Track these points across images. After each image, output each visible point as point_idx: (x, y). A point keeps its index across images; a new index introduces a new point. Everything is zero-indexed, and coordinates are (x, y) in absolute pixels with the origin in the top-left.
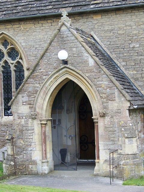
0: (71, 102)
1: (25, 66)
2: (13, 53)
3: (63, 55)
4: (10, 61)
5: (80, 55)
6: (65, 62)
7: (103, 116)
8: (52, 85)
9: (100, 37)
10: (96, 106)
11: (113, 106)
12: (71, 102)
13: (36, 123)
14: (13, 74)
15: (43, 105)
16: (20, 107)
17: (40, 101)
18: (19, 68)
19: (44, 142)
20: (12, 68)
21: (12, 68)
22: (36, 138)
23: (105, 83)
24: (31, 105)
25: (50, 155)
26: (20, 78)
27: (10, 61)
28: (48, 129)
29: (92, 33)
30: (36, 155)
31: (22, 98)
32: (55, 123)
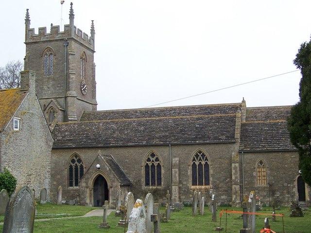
0: (100, 181)
1: (84, 166)
2: (79, 161)
3: (98, 166)
4: (78, 164)
5: (104, 166)
6: (99, 168)
7: (111, 187)
8: (94, 176)
9: (114, 157)
10: (109, 184)
11: (115, 184)
12: (100, 181)
13: (88, 189)
14: (74, 170)
15: (91, 183)
16: (83, 184)
17: (90, 181)
18: (82, 167)
19: (91, 196)
20: (74, 167)
21: (79, 167)
22: (88, 195)
23: (112, 176)
24: (87, 183)
25: (92, 201)
26: (82, 175)
27: (78, 164)
28: (92, 192)
29: (111, 155)
30: (88, 201)
31: (83, 180)
32: (95, 190)
